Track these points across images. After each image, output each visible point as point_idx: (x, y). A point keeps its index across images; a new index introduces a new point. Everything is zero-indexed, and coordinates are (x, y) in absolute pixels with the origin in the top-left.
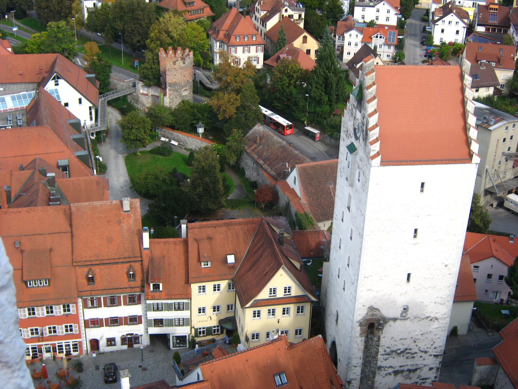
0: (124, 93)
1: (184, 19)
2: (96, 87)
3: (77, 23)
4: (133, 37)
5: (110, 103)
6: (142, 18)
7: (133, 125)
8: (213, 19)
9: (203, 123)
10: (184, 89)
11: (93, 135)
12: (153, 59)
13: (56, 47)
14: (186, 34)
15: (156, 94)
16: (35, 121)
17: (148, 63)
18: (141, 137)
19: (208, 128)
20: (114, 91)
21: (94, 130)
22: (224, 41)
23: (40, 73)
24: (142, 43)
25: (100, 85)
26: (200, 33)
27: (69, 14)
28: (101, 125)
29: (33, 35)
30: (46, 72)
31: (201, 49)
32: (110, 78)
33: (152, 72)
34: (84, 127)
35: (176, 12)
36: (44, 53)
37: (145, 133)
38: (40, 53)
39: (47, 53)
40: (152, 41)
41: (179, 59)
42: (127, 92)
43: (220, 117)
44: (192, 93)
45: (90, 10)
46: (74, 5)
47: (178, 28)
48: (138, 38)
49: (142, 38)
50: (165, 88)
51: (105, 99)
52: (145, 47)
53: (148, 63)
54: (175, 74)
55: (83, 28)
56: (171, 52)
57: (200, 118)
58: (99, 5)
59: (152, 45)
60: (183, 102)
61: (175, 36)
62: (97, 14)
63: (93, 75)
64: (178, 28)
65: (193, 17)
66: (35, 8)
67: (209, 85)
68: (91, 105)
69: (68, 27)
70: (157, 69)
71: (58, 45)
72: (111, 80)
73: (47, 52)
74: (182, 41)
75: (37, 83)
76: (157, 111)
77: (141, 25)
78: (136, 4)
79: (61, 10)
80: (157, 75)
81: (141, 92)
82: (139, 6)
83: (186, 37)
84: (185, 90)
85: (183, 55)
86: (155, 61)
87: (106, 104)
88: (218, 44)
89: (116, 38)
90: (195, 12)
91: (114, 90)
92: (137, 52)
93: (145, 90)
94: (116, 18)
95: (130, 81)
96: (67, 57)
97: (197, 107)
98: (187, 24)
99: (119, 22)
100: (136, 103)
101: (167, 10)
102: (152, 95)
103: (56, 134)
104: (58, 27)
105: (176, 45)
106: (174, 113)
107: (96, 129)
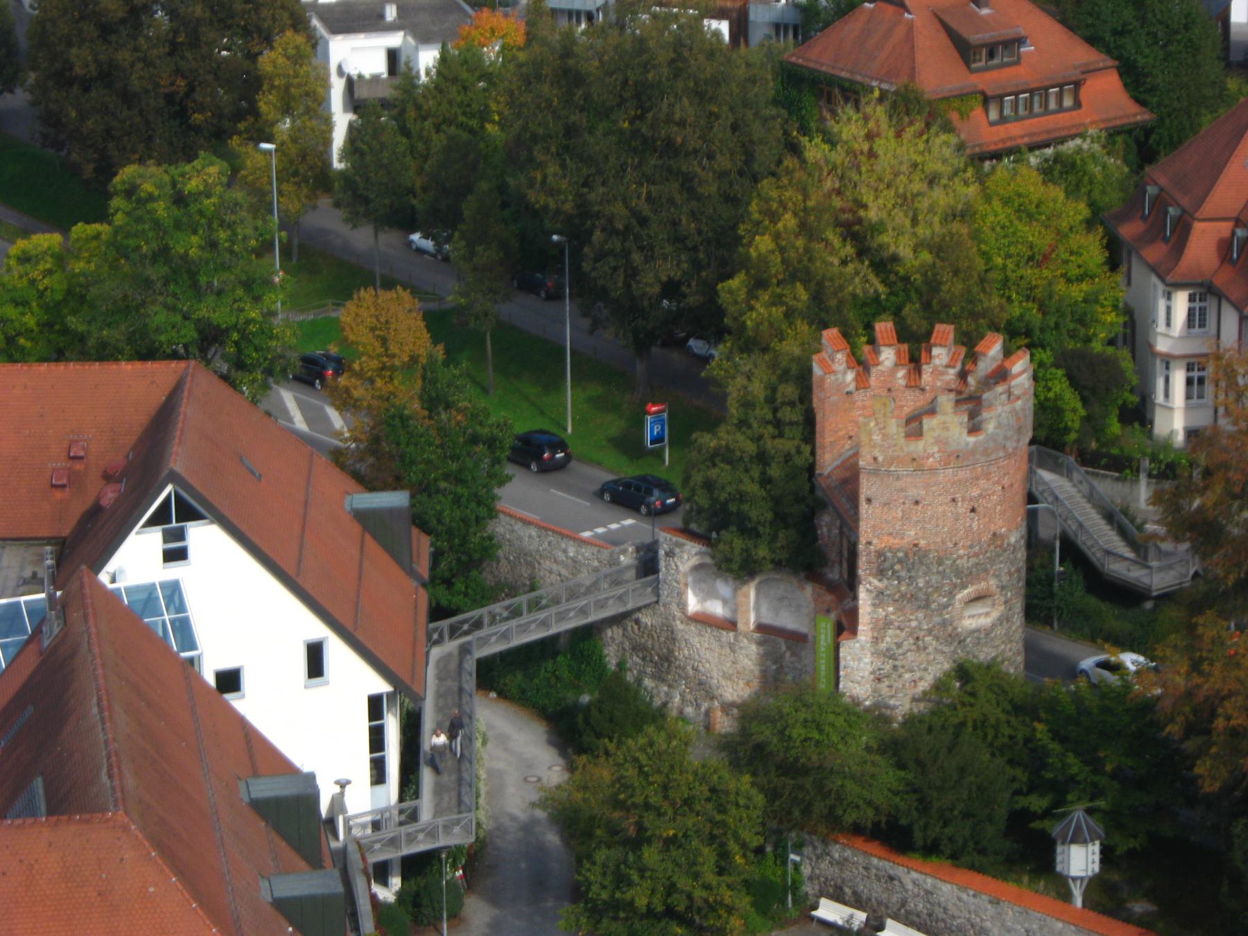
0: (583, 611)
1: (960, 147)
2: (411, 573)
3: (289, 172)
4: (637, 257)
5: (493, 675)
6: (694, 143)
7: (649, 819)
8: (1143, 147)
9: (1089, 811)
10: (969, 591)
11: (383, 879)
12: (770, 400)
13: (158, 316)
14: (976, 236)
15: (788, 621)
16: (39, 783)
17: (743, 423)
18: (699, 893)
19: (1123, 845)
20: (522, 599)
21: (393, 842)
22: (1218, 282)
23: (74, 481)
24: (693, 300)
25: (436, 556)
26: (1062, 235)
27: (239, 116)
28: (438, 812)
29: (21, 244)
30: (108, 477)
31: (1073, 335)
32: (493, 514)
33: (765, 481)
34: (331, 822)
35: (905, 105)
36: (85, 356)
37: (721, 871)
38: (59, 355)
39: (101, 358)
40: (759, 283)
41: (946, 402)
42: (601, 605)
43: (1209, 774)
44: (1018, 619)
45: (361, 93)
46: (270, 60)
47: (924, 204)
48: (668, 269)
49: (697, 266)
50: (852, 583)
51: (465, 650)
52: (712, 321)
53: (743, 423)
54: (913, 493)
55: (325, 202)
56: (888, 356)
57: (1072, 779)
58: (427, 58)
59: (761, 313)
60: (963, 672)
61: (904, 250)
62: (411, 113)
63: (396, 499)
64: (924, 204)
65: (1016, 131)
66: (32, 77)
67: (1121, 565)
68: (381, 686)
69: (239, 195)
70: (799, 461)
71: (172, 309)
72: (500, 528)
73: (105, 353)
74: (952, 288)
75: (49, 540)
76: (797, 732)
77: (688, 184)
78: (664, 56)
79: (191, 89)
80: (799, 499)
81: (693, 603)
82: (678, 65)
83: (980, 264)
84: (978, 598)
85: (963, 375)
86: (787, 414)
87: (470, 682)
88: (1181, 302)
89: (531, 263)
90: (1029, 105)
91: (520, 589)
92: (655, 350)
93: (710, 594)
94: (535, 139)
95: (613, 541)
96: (224, 378)
97: (1052, 706)
98: (981, 179)
99: (553, 169)
100: (659, 677)
101: (852, 93)
102: (761, 628)
103: (180, 871)
104: (180, 200)
105: (911, 311)
106: (901, 744)
107: (411, 839)
